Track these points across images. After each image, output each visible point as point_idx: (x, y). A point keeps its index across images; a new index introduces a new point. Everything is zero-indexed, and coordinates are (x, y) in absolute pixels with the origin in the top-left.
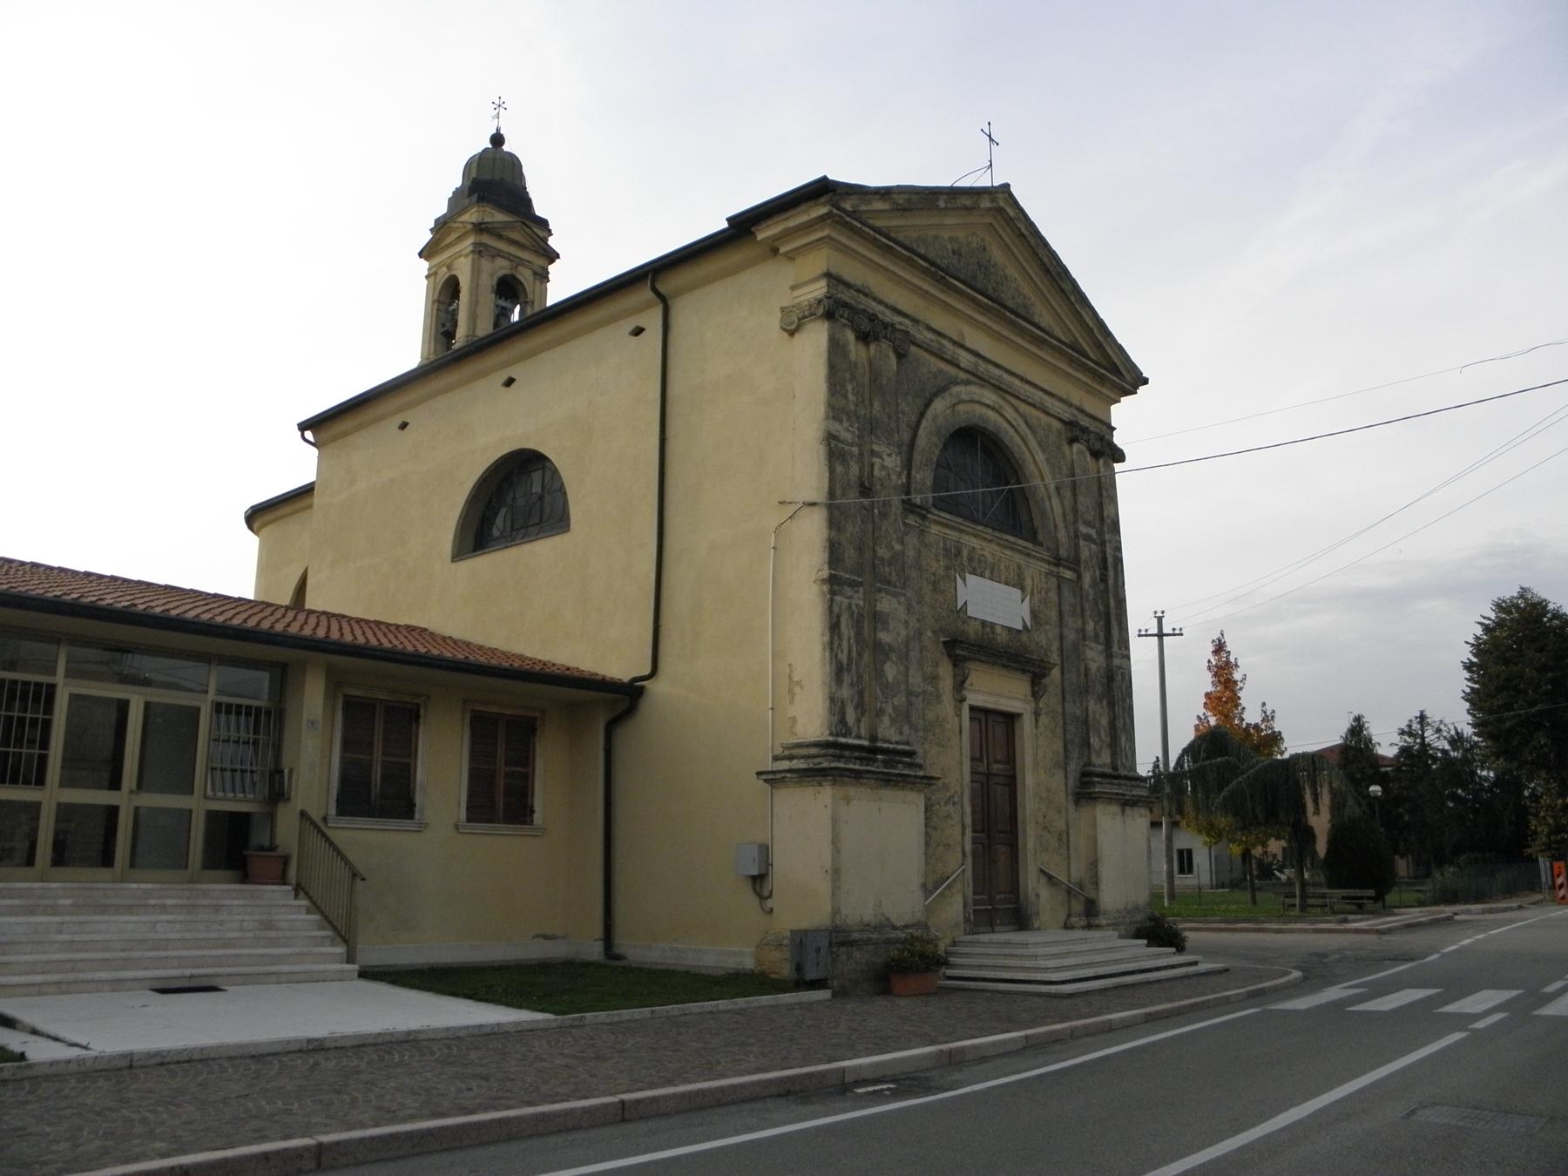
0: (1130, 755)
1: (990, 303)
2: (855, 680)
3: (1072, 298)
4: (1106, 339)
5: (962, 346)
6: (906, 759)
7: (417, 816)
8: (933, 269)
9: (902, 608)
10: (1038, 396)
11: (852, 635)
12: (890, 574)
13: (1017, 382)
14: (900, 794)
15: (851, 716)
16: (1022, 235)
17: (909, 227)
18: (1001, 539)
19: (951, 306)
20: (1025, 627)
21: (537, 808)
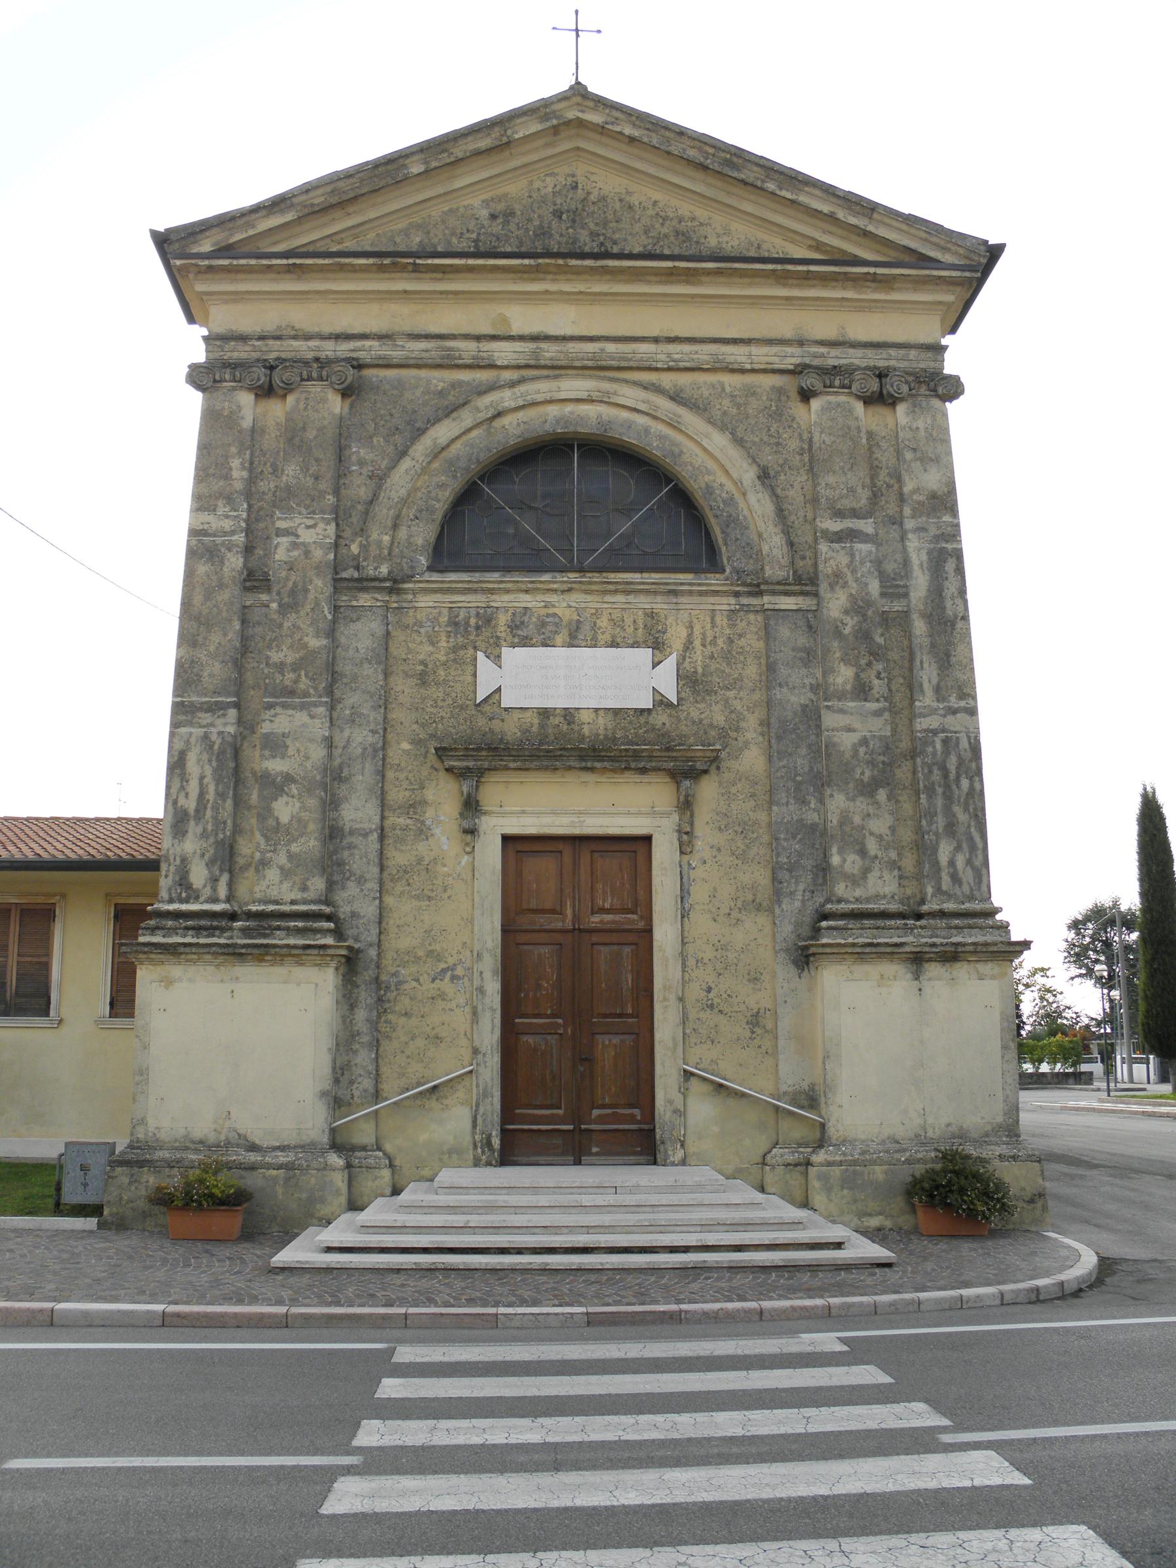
0: (967, 876)
2: (210, 827)
3: (771, 186)
10: (704, 353)
11: (208, 771)
14: (279, 971)
16: (632, 140)
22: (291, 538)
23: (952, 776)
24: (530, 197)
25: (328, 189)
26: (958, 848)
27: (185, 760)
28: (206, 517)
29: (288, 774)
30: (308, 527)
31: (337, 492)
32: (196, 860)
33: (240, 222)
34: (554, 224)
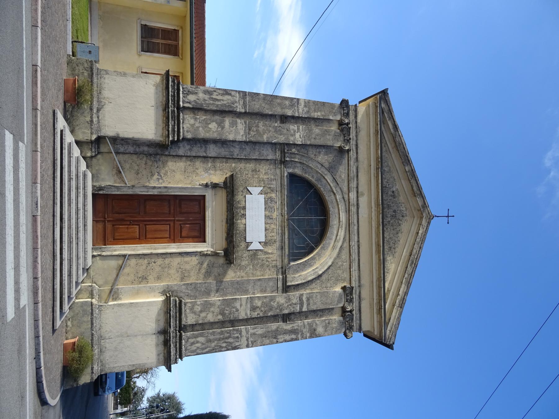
2: (207, 102)
3: (406, 276)
6: (176, 127)
7: (143, 53)
10: (355, 256)
11: (225, 102)
16: (418, 233)
17: (394, 160)
19: (371, 183)
30: (300, 136)
32: (196, 97)
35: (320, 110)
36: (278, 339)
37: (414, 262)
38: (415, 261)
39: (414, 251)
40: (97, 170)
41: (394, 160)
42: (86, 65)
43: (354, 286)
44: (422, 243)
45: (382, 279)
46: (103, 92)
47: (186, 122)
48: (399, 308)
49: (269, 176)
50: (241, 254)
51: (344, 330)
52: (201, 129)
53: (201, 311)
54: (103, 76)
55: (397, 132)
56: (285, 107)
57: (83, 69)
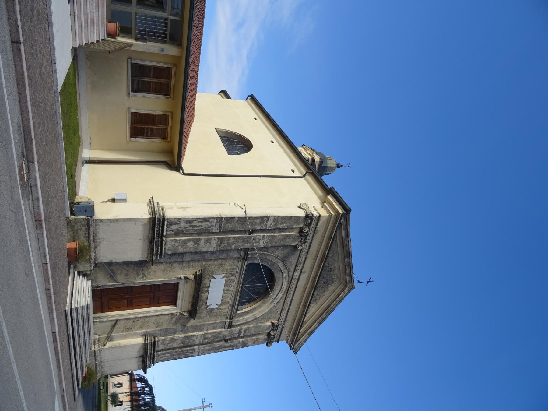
0: (162, 359)
1: (316, 282)
2: (187, 229)
3: (320, 318)
4: (308, 334)
5: (301, 272)
6: (159, 251)
7: (132, 93)
8: (325, 257)
9: (211, 249)
10: (286, 307)
11: (203, 227)
12: (224, 244)
13: (291, 297)
15: (174, 227)
18: (238, 293)
19: (314, 267)
20: (208, 306)
21: (137, 139)
22: (261, 239)
23: (184, 354)
24: (333, 274)
25: (348, 245)
26: (168, 357)
27: (207, 222)
28: (272, 220)
29: (200, 244)
30: (264, 242)
31: (272, 247)
32: (178, 226)
33: (346, 228)
34: (326, 279)
35: (286, 222)
36: (210, 404)
37: (329, 312)
38: (330, 311)
39: (332, 306)
40: (95, 277)
41: (338, 251)
42: (83, 223)
43: (280, 324)
44: (339, 302)
45: (304, 313)
46: (98, 235)
47: (168, 244)
48: (308, 335)
49: (232, 267)
50: (202, 312)
51: (267, 342)
52: (180, 247)
53: (169, 343)
54: (98, 224)
55: (347, 239)
56: (255, 224)
57: (81, 226)
